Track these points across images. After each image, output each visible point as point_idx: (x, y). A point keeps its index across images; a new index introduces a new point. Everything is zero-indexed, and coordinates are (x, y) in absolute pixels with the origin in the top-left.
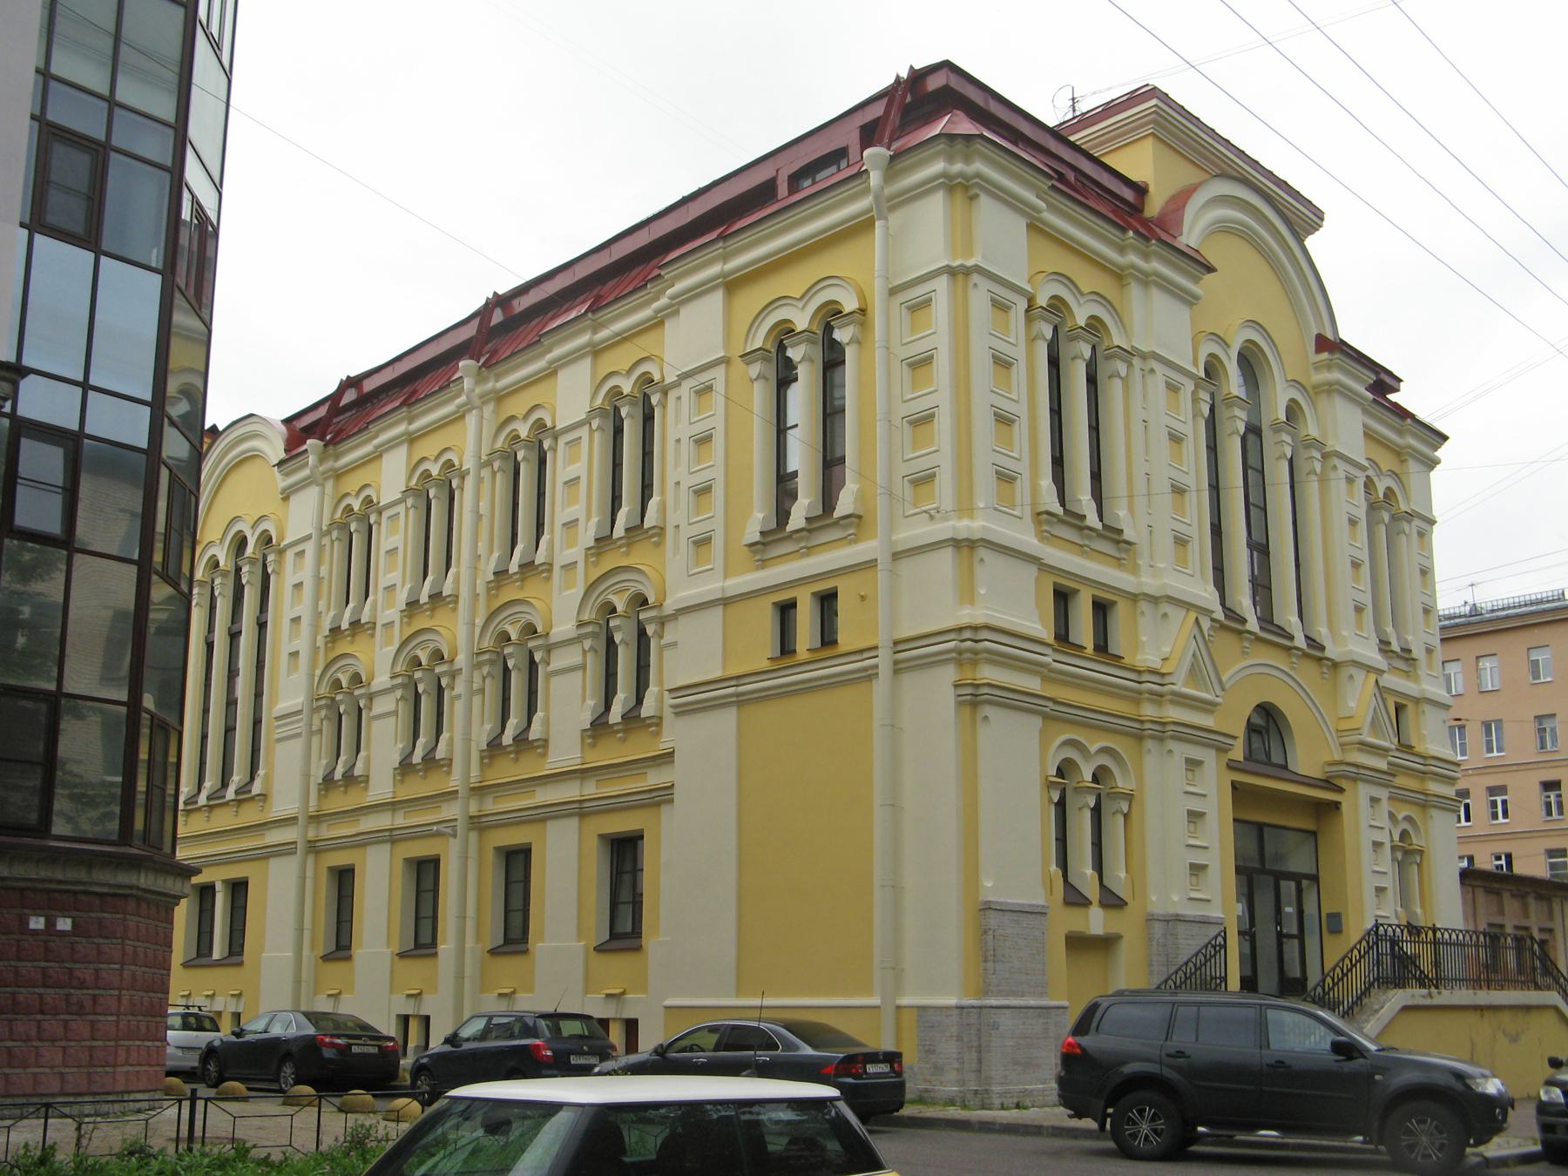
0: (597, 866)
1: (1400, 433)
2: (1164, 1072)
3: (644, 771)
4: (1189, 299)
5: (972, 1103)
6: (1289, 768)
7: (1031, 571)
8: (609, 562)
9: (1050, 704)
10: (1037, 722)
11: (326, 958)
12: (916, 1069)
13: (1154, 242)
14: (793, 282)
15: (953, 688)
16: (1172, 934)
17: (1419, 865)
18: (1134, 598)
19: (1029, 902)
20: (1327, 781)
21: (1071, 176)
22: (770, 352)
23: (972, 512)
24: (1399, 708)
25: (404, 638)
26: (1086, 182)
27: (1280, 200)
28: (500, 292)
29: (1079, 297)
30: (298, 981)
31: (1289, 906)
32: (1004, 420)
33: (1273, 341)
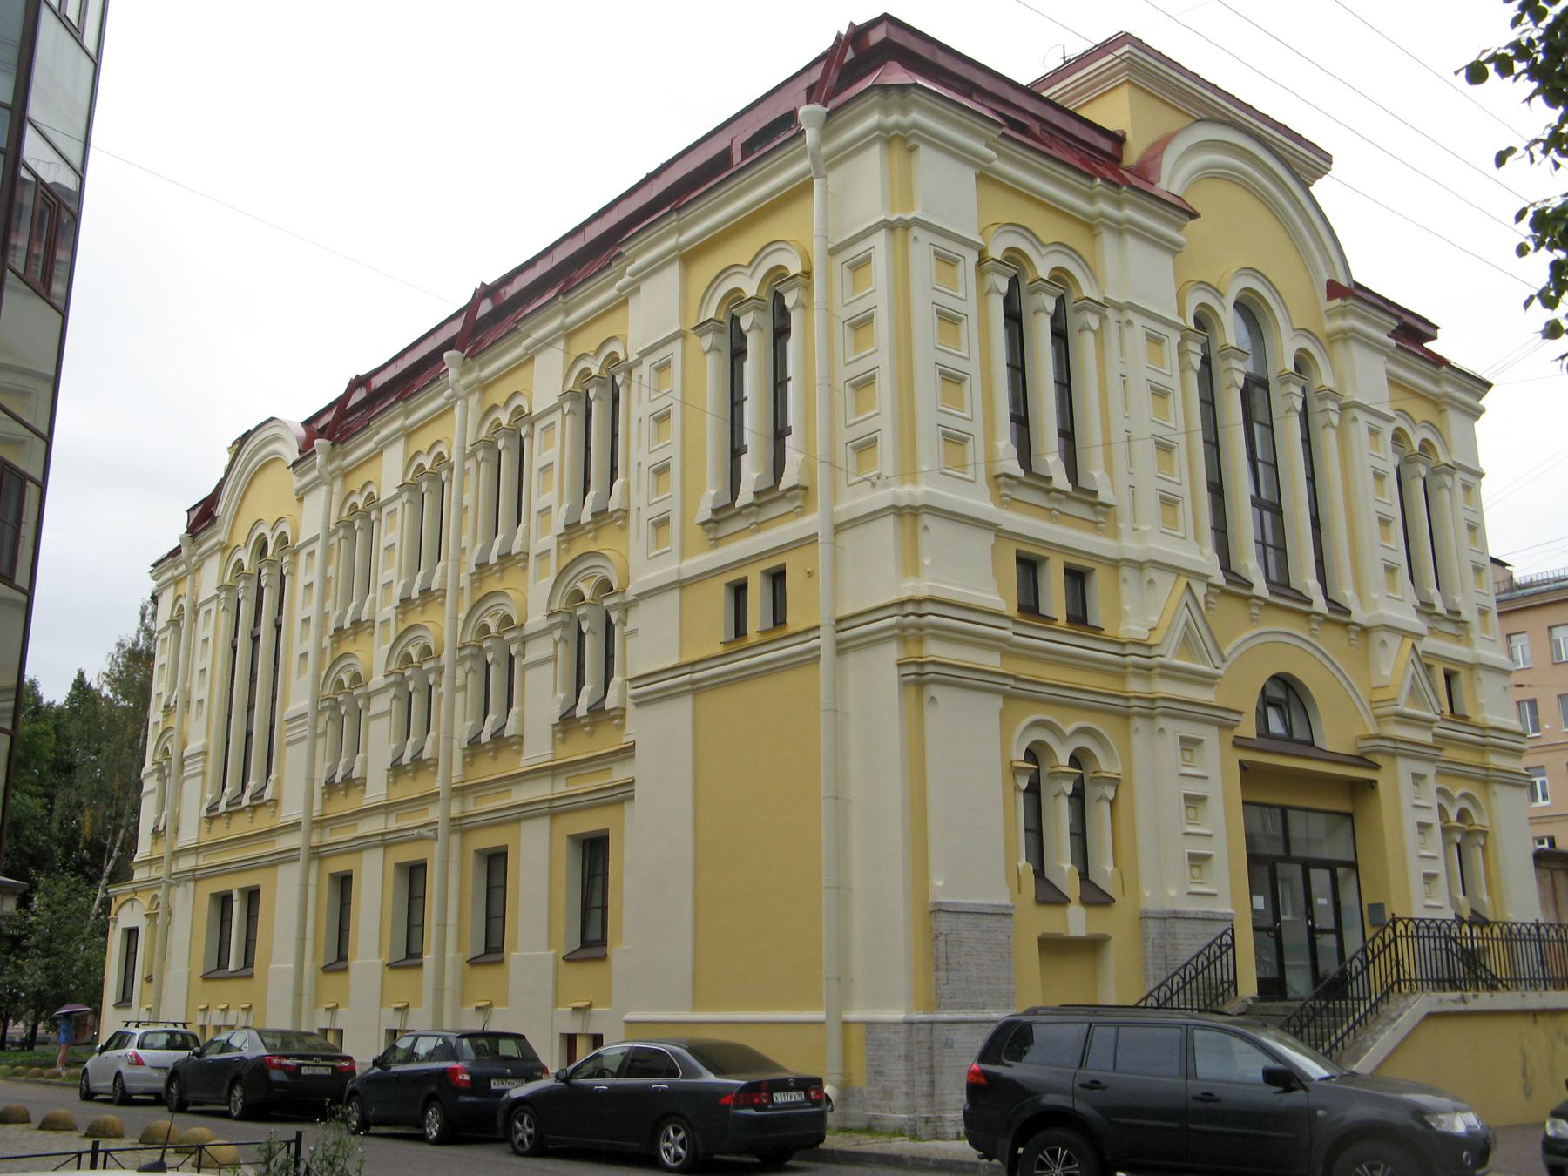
0: (567, 869)
1: (1437, 382)
2: (1076, 1108)
3: (608, 767)
4: (1172, 248)
5: (923, 1132)
6: (1316, 744)
7: (989, 538)
8: (579, 548)
9: (1011, 682)
10: (997, 702)
11: (474, 962)
12: (865, 1092)
13: (1125, 188)
14: (740, 251)
15: (896, 668)
16: (1169, 934)
17: (1484, 848)
18: (1115, 564)
19: (989, 902)
20: (1360, 757)
21: (1036, 127)
22: (722, 323)
23: (916, 477)
24: (1449, 677)
25: (399, 633)
26: (1053, 132)
27: (1274, 140)
28: (488, 283)
29: (1039, 247)
30: (298, 995)
31: (1322, 897)
32: (951, 378)
33: (1271, 283)
